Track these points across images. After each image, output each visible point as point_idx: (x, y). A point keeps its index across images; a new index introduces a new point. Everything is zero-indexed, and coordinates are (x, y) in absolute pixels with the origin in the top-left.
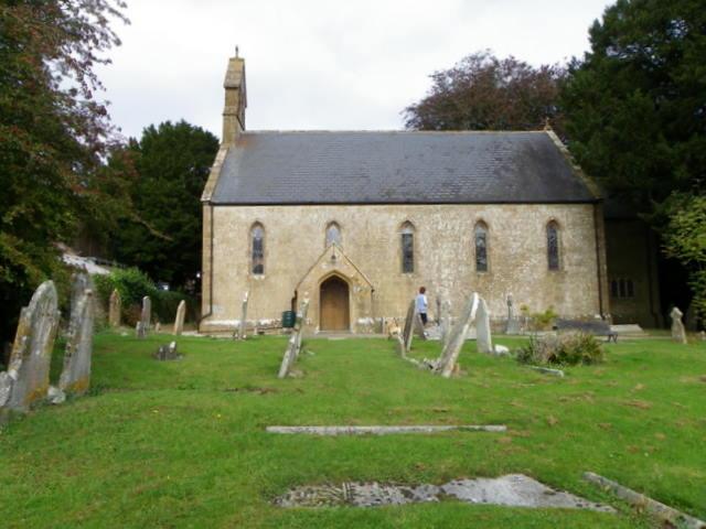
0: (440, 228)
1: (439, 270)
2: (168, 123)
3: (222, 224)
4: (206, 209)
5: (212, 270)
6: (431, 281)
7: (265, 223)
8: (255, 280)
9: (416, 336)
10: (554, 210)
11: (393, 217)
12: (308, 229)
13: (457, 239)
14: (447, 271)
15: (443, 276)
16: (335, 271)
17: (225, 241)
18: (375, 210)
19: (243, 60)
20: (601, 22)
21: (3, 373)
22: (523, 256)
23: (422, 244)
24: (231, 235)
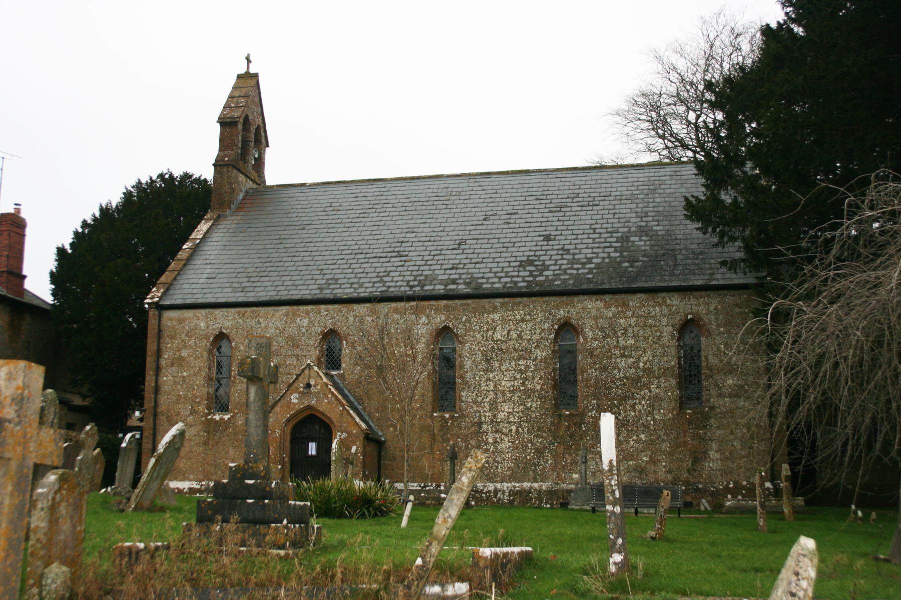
0: (498, 336)
1: (494, 406)
2: (139, 182)
3: (173, 338)
4: (153, 313)
5: (156, 405)
6: (480, 424)
7: (233, 334)
8: (216, 422)
9: (800, 501)
10: (693, 301)
11: (424, 319)
12: (293, 342)
13: (526, 353)
14: (507, 408)
15: (501, 416)
16: (309, 407)
17: (179, 362)
18: (396, 311)
19: (256, 76)
20: (54, 270)
21: (769, 599)
22: (636, 380)
23: (468, 364)
24: (184, 353)
